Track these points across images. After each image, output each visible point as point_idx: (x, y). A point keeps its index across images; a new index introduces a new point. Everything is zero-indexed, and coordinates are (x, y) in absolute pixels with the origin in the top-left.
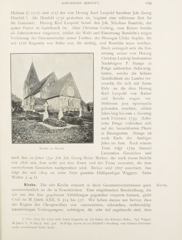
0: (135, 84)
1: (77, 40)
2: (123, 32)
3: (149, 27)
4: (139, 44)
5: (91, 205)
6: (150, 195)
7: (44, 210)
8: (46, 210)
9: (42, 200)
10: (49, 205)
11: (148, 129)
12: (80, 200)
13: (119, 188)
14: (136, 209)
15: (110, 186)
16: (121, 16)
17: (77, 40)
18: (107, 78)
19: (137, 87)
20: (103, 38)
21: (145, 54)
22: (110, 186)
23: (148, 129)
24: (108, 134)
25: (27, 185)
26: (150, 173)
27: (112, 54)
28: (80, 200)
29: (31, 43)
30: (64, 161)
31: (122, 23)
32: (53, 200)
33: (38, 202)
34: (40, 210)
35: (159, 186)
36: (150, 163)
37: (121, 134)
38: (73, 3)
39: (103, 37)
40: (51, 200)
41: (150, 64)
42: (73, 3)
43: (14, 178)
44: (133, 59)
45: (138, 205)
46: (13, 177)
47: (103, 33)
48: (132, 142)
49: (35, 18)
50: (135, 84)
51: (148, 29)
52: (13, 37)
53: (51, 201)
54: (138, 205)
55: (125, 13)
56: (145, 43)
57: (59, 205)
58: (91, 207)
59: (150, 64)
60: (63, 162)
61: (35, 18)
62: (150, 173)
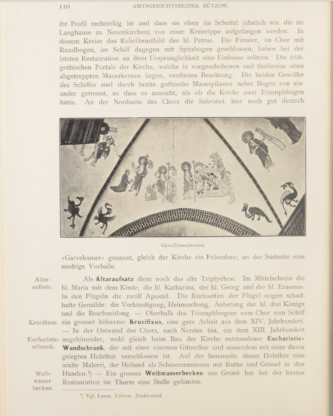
1: (77, 309)
2: (259, 82)
7: (121, 76)
9: (162, 41)
10: (266, 313)
16: (217, 195)
17: (77, 309)
20: (124, 366)
30: (130, 344)
32: (262, 331)
33: (175, 37)
34: (93, 267)
39: (124, 363)
40: (257, 330)
45: (107, 331)
47: (108, 374)
49: (88, 280)
50: (166, 50)
52: (94, 265)
55: (293, 101)
58: (205, 28)
60: (128, 346)
61: (88, 280)
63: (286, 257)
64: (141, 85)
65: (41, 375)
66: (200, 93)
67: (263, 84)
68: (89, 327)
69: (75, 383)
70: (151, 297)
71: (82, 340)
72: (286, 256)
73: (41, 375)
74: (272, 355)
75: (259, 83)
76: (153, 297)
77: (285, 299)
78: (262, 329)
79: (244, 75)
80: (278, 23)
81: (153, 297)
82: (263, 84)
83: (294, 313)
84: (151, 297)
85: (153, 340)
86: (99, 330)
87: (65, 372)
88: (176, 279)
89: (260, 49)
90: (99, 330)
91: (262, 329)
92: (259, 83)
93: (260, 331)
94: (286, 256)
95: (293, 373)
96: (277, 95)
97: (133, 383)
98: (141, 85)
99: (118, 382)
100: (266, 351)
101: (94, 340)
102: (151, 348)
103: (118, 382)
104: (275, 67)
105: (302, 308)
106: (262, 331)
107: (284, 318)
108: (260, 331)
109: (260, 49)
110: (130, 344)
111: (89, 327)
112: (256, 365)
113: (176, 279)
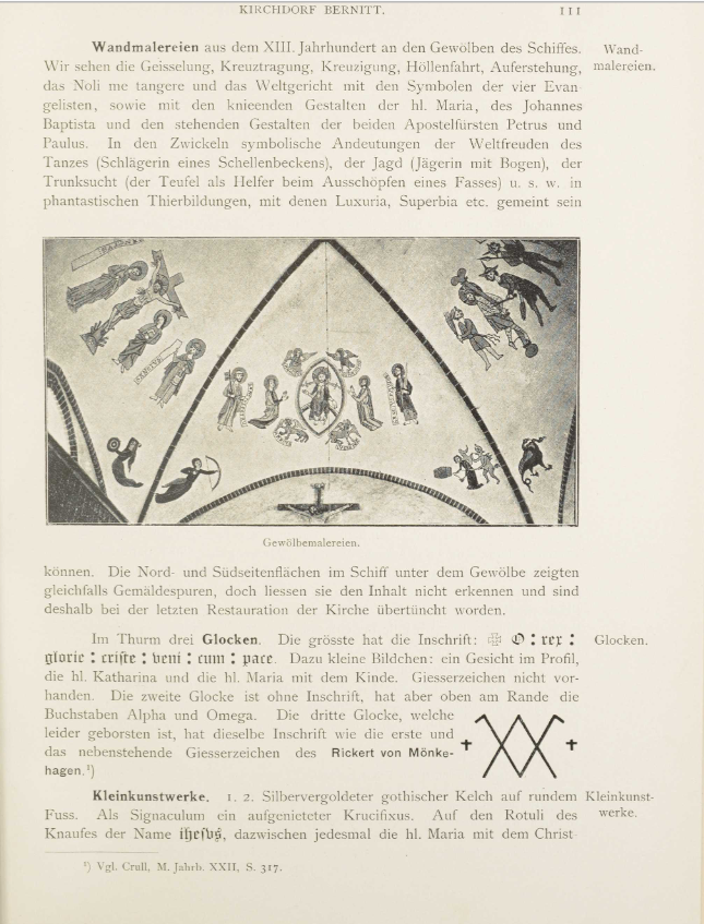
0: (474, 165)
5: (232, 755)
8: (234, 107)
12: (267, 868)
13: (259, 584)
19: (301, 689)
24: (48, 126)
25: (102, 795)
27: (442, 105)
28: (267, 868)
31: (243, 611)
32: (286, 49)
37: (456, 107)
38: (212, 660)
41: (578, 184)
42: (212, 660)
45: (164, 797)
48: (145, 831)
50: (474, 165)
53: (275, 54)
54: (164, 797)
59: (578, 184)
60: (271, 199)
63: (347, 641)
65: (269, 88)
67: (514, 165)
69: (334, 106)
70: (415, 126)
72: (348, 637)
73: (269, 88)
76: (421, 126)
77: (510, 684)
78: (286, 45)
81: (421, 126)
82: (514, 165)
83: (114, 164)
84: (415, 126)
85: (286, 183)
87: (412, 64)
88: (507, 49)
89: (188, 735)
91: (286, 45)
93: (280, 49)
94: (348, 637)
95: (172, 611)
96: (565, 73)
99: (156, 200)
100: (378, 649)
103: (156, 200)
104: (175, 799)
105: (48, 193)
106: (286, 49)
107: (83, 174)
108: (280, 49)
109: (188, 735)
112: (575, 592)
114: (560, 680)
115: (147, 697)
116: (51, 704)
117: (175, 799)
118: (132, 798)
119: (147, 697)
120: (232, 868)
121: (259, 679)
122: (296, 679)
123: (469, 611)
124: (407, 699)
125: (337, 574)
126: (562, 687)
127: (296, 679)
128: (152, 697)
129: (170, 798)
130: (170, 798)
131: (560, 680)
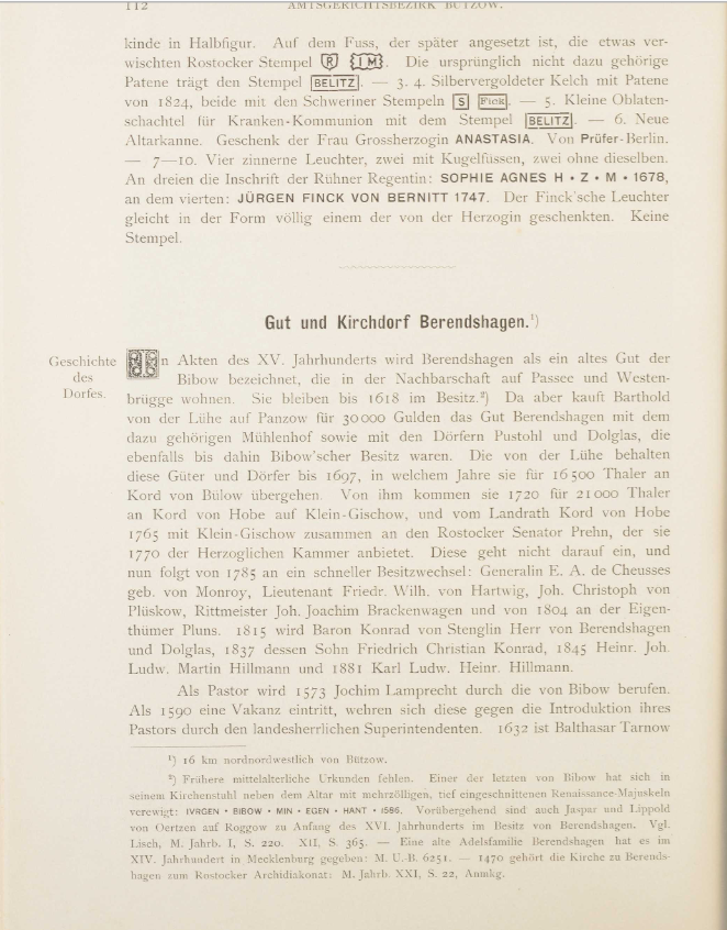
3: (628, 414)
4: (338, 104)
6: (661, 139)
11: (643, 729)
14: (367, 688)
15: (455, 360)
18: (139, 61)
21: (222, 555)
22: (455, 360)
23: (643, 729)
26: (664, 217)
29: (377, 179)
30: (615, 73)
35: (575, 102)
36: (662, 417)
43: (624, 380)
44: (205, 103)
45: (501, 591)
46: (622, 375)
48: (407, 376)
51: (436, 480)
54: (501, 591)
56: (651, 454)
57: (287, 219)
61: (189, 362)
62: (664, 217)
64: (131, 401)
65: (631, 380)
66: (148, 593)
68: (464, 409)
71: (195, 439)
73: (631, 380)
74: (575, 156)
75: (317, 629)
79: (476, 455)
80: (489, 458)
85: (622, 690)
86: (160, 827)
88: (472, 779)
90: (160, 827)
92: (317, 629)
97: (666, 418)
98: (131, 401)
101: (277, 730)
102: (638, 417)
110: (615, 73)
111: (464, 409)
113: (472, 779)
114: (653, 592)
115: (382, 160)
116: (132, 72)
117: (549, 161)
118: (159, 614)
119: (382, 160)
120: (313, 843)
121: (190, 670)
122: (396, 496)
123: (614, 514)
124: (581, 361)
125: (153, 632)
126: (653, 426)
127: (396, 496)
128: (387, 160)
129: (616, 42)
130: (616, 42)
131: (653, 592)
